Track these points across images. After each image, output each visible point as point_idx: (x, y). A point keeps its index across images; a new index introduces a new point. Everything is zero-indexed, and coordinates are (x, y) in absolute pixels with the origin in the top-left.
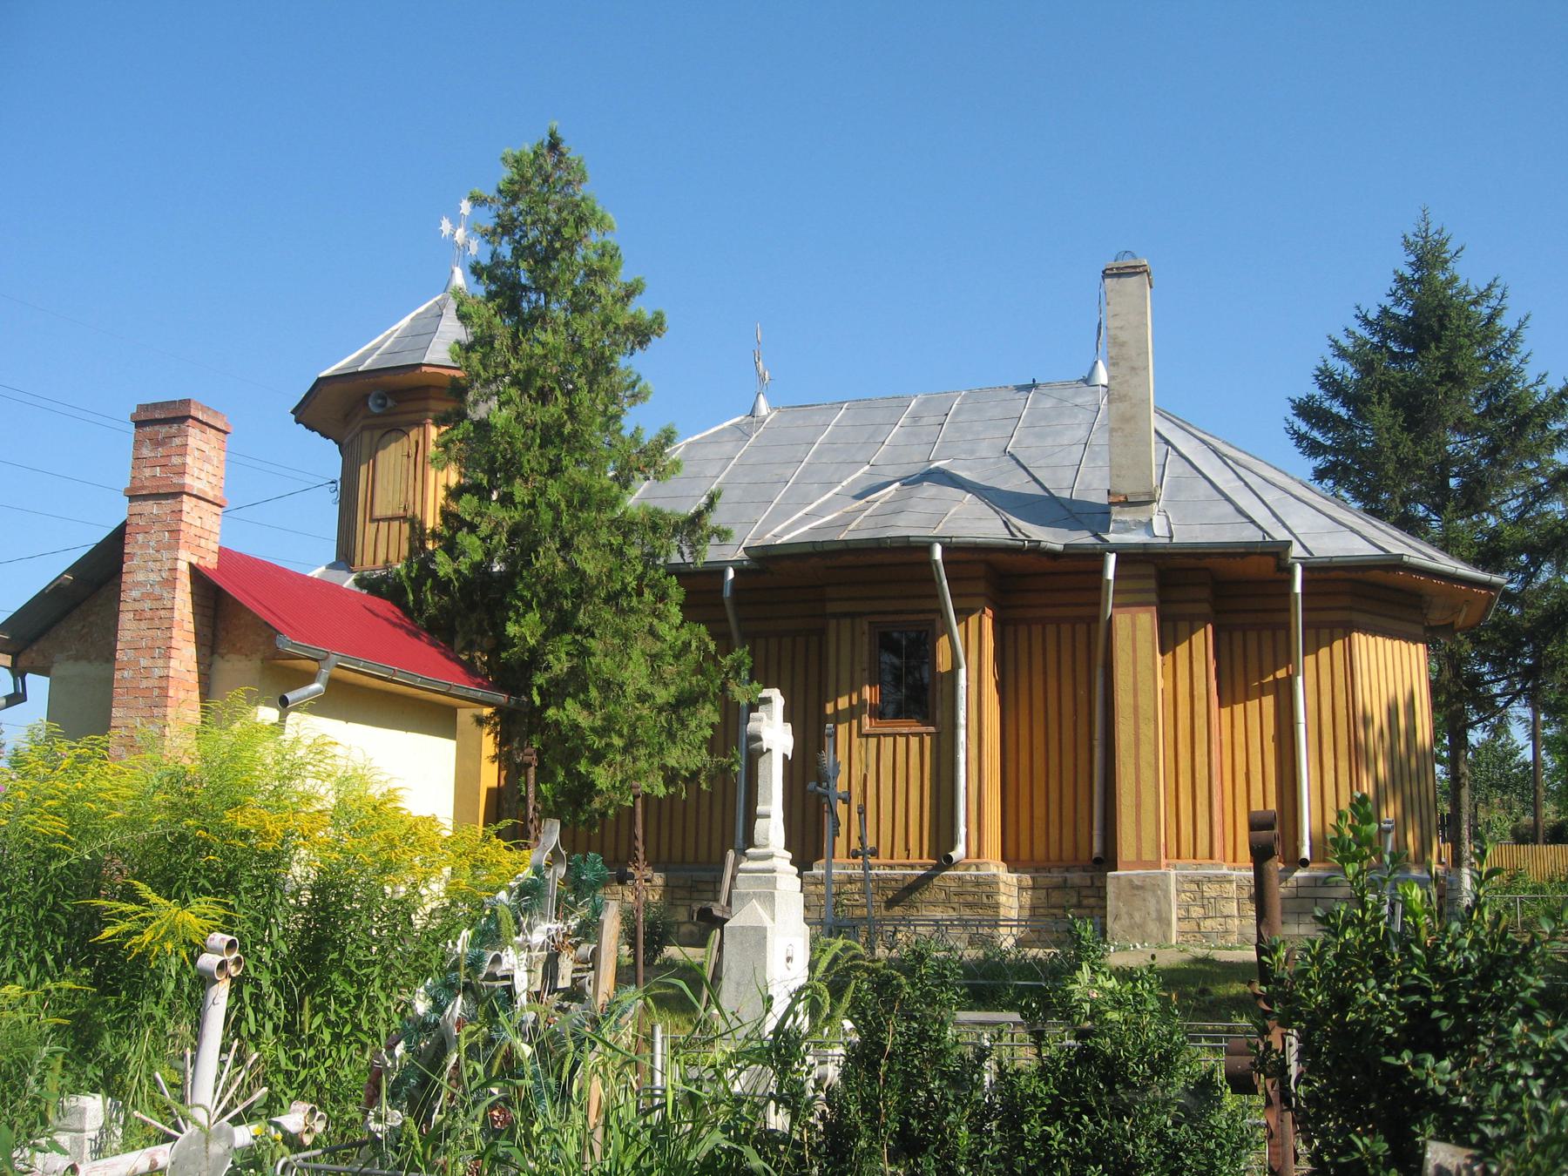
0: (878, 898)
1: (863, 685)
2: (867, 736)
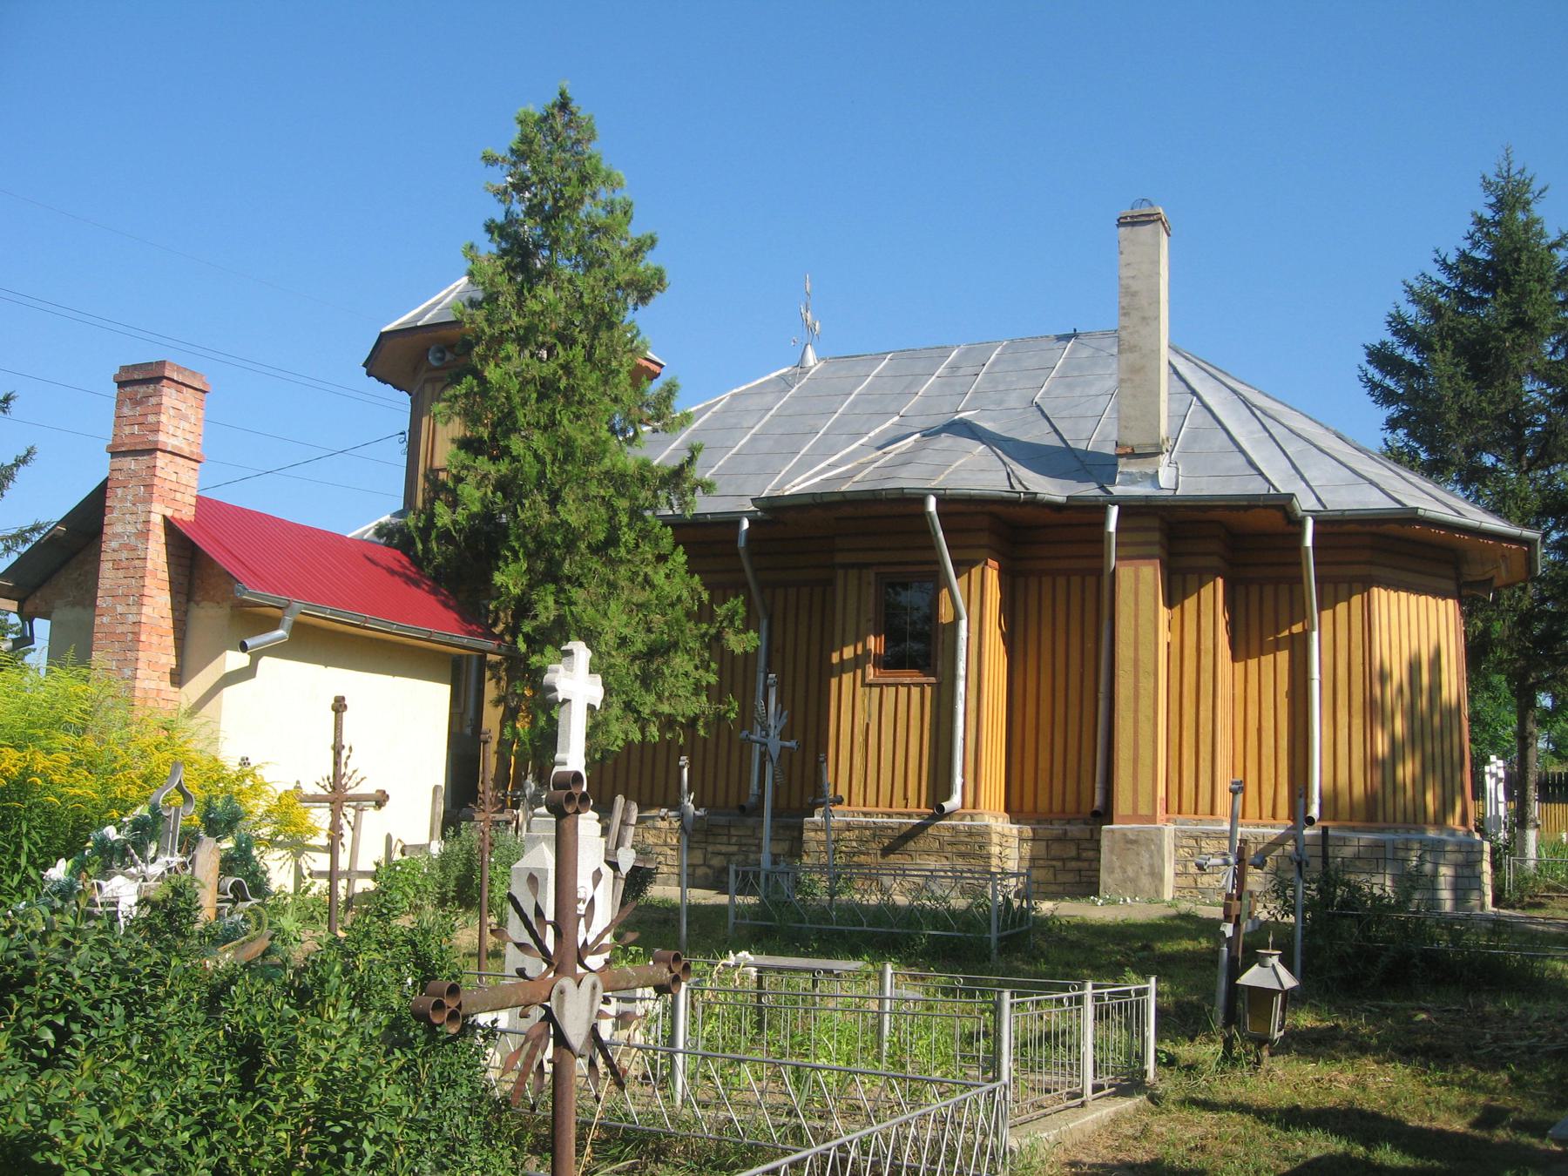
0: (874, 846)
1: (868, 635)
2: (870, 685)
